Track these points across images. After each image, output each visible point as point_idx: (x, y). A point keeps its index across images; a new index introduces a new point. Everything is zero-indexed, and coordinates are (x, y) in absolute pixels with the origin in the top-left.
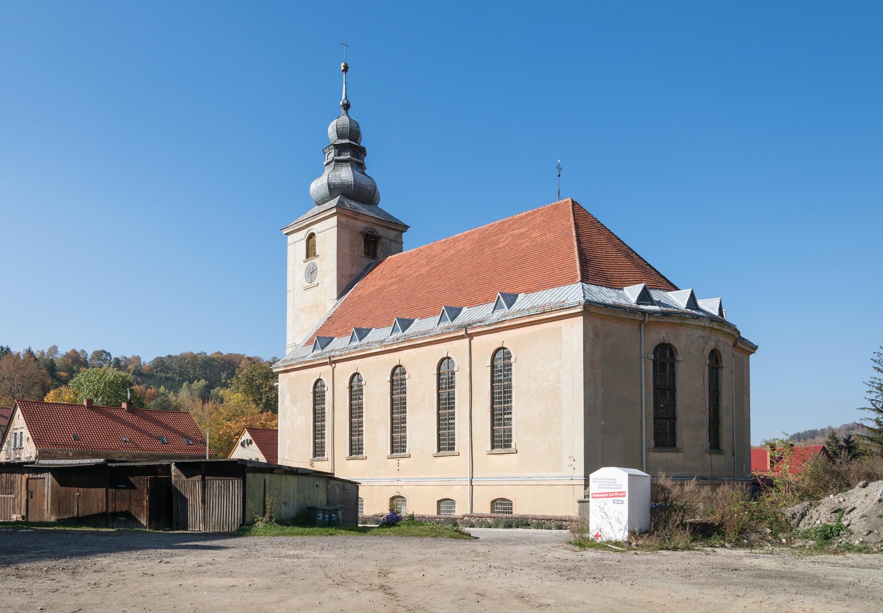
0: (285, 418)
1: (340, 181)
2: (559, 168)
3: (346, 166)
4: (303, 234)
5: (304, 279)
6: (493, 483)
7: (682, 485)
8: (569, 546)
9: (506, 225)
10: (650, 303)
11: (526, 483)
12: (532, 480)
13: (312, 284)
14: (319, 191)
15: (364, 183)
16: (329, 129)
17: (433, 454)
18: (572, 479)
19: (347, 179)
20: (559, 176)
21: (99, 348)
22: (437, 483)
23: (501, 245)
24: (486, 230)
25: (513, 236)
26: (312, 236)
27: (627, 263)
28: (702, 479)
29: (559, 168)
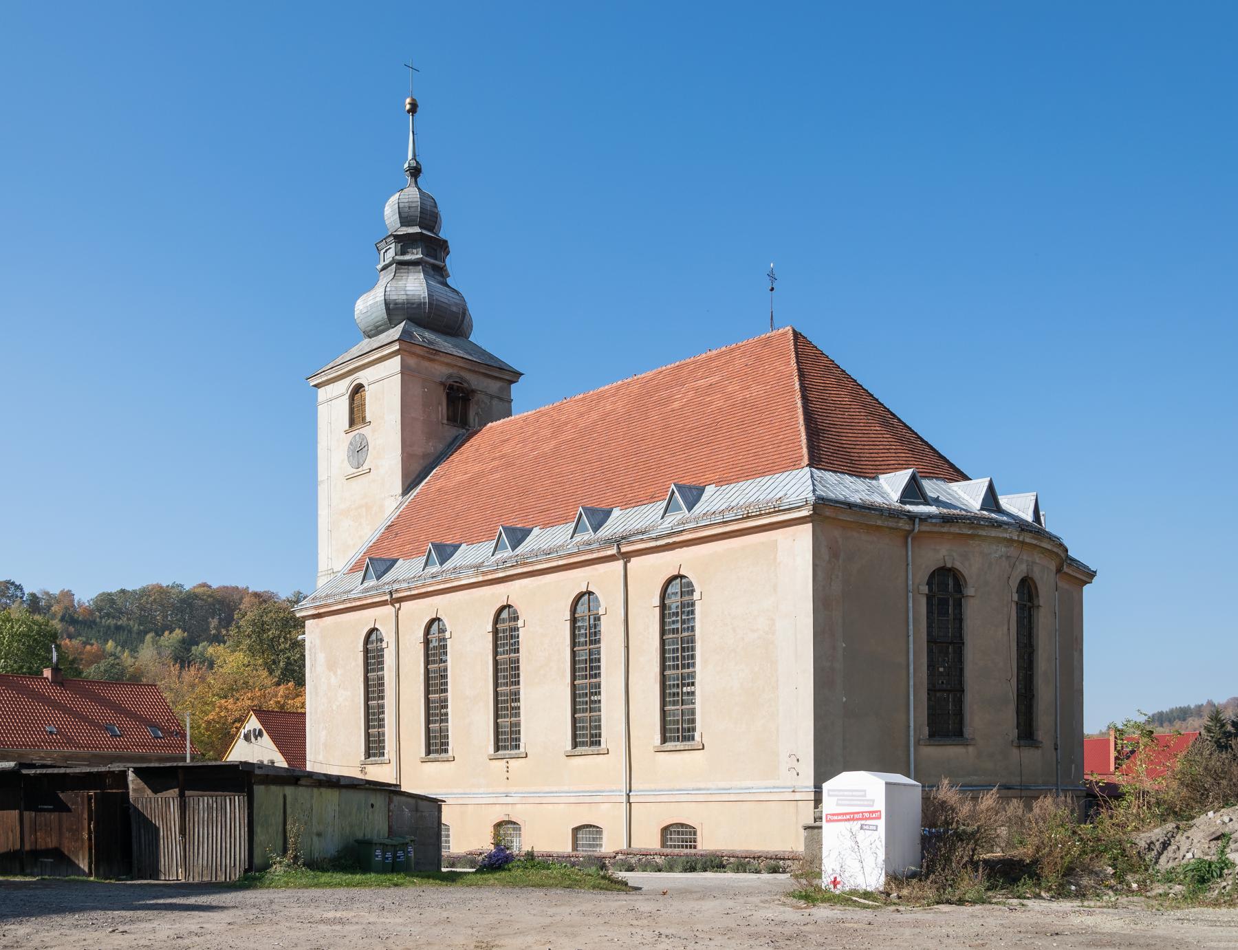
1: (405, 297)
2: (772, 276)
5: (346, 461)
9: (686, 371)
18: (793, 791)
19: (417, 293)
20: (772, 289)
22: (573, 800)
26: (358, 389)
27: (884, 436)
29: (772, 276)
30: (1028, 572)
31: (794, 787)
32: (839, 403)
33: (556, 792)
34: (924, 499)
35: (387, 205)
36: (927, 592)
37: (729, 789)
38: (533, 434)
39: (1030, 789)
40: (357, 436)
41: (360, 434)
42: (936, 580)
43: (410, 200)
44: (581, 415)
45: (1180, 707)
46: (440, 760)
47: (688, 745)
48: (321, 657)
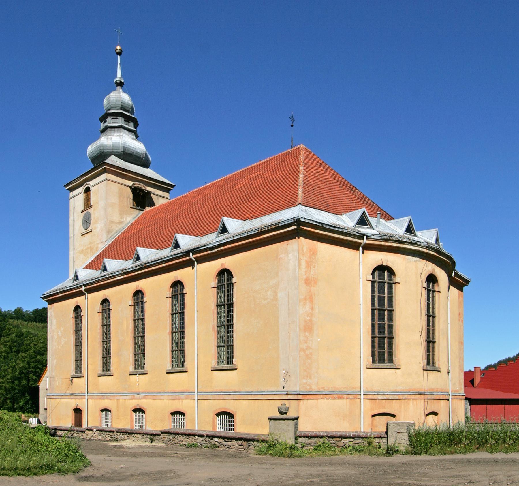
0: (52, 340)
1: (111, 144)
2: (292, 119)
3: (118, 132)
4: (81, 189)
5: (82, 226)
6: (217, 397)
7: (10, 399)
8: (190, 483)
9: (247, 172)
10: (369, 227)
11: (245, 397)
12: (252, 395)
13: (88, 230)
14: (94, 152)
15: (134, 147)
16: (104, 101)
17: (166, 370)
18: (287, 394)
19: (118, 142)
20: (292, 126)
21: (36, 308)
22: (171, 397)
23: (239, 187)
24: (230, 178)
25: (250, 179)
26: (88, 190)
27: (350, 196)
28: (419, 394)
29: (292, 119)
30: (432, 272)
31: (288, 391)
32: (334, 198)
33: (264, 392)
34: (370, 226)
35: (105, 99)
36: (371, 279)
37: (251, 392)
38: (171, 208)
39: (379, 394)
40: (87, 214)
41: (87, 212)
42: (377, 273)
43: (116, 97)
44: (194, 197)
45: (503, 360)
46: (107, 375)
47: (229, 366)
48: (54, 321)
